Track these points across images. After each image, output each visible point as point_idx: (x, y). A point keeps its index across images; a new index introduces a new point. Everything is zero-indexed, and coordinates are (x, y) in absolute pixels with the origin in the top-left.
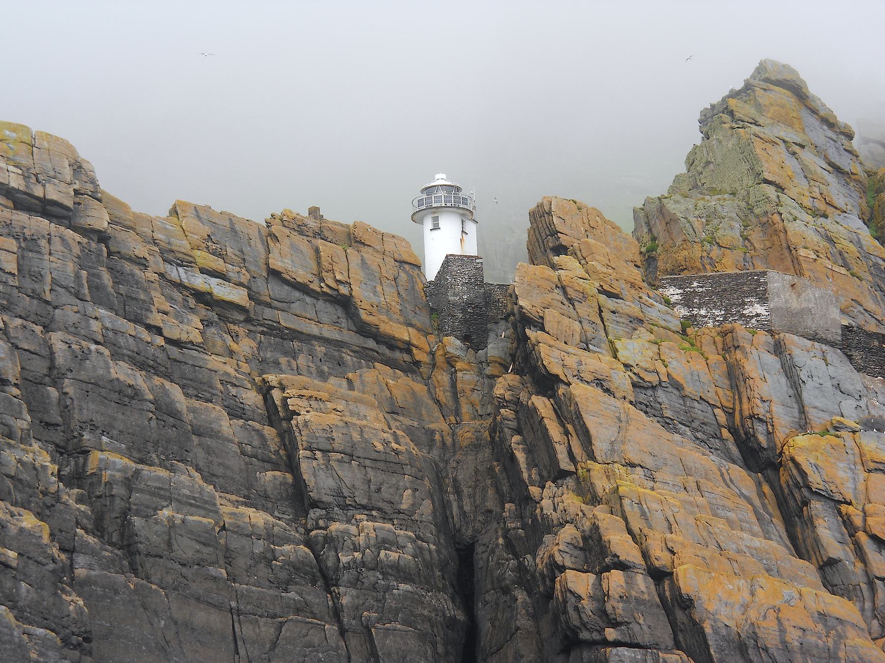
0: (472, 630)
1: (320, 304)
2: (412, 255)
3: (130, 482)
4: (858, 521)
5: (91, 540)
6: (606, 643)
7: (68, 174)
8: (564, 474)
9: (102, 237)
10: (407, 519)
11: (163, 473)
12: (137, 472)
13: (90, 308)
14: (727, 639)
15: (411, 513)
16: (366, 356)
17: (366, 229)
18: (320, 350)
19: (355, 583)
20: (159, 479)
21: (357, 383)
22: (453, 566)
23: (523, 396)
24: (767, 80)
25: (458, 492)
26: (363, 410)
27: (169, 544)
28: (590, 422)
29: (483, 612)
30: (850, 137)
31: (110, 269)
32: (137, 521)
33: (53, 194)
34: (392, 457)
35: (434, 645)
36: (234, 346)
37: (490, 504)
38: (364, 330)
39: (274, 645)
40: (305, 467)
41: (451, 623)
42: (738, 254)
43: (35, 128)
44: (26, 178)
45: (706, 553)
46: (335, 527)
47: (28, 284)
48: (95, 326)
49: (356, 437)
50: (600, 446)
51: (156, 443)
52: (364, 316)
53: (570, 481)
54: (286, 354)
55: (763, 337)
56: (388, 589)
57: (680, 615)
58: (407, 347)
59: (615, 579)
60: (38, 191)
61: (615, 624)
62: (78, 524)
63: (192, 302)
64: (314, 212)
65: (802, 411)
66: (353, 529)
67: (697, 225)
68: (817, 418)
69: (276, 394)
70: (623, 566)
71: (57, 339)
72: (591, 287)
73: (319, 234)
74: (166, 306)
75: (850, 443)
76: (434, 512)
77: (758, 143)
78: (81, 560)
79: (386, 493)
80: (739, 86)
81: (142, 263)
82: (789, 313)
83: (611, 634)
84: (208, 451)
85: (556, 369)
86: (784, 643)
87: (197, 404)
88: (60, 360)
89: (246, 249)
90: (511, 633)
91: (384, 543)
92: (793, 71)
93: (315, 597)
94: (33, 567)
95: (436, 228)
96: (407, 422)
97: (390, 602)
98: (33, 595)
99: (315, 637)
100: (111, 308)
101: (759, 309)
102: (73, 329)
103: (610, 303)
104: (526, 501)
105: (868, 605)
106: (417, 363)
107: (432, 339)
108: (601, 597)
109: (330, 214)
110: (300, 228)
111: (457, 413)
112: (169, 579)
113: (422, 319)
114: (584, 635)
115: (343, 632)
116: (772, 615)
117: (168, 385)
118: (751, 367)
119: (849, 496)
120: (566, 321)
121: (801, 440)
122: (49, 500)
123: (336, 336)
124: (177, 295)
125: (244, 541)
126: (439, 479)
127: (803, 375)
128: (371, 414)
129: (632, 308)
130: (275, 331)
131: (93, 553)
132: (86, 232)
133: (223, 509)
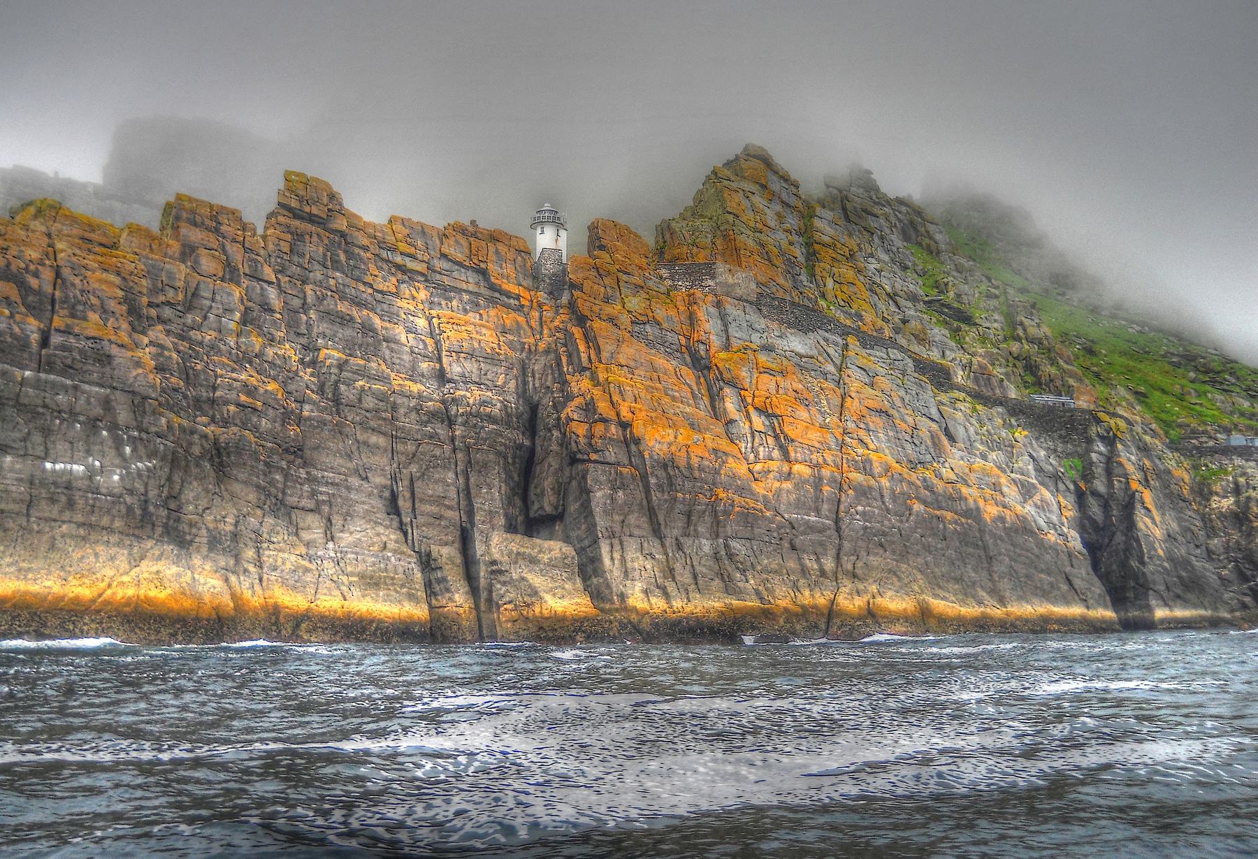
1: (469, 273)
2: (526, 247)
3: (341, 366)
4: (749, 400)
5: (314, 396)
6: (590, 461)
7: (325, 200)
9: (343, 235)
11: (362, 362)
12: (347, 361)
13: (330, 273)
14: (657, 461)
15: (502, 387)
16: (492, 302)
18: (466, 297)
21: (485, 317)
22: (526, 416)
23: (569, 326)
25: (533, 376)
26: (484, 331)
27: (360, 400)
28: (601, 342)
29: (538, 441)
31: (346, 252)
32: (343, 387)
33: (315, 211)
35: (505, 458)
37: (548, 384)
38: (493, 288)
39: (414, 455)
40: (445, 360)
42: (708, 252)
43: (309, 175)
45: (654, 415)
46: (458, 393)
47: (296, 259)
48: (332, 282)
49: (476, 345)
50: (605, 355)
52: (493, 279)
53: (588, 373)
54: (446, 299)
55: (710, 298)
56: (483, 427)
58: (518, 297)
59: (599, 429)
60: (307, 209)
61: (596, 451)
62: (307, 387)
63: (393, 270)
64: (473, 222)
65: (728, 339)
66: (468, 395)
67: (687, 235)
68: (736, 344)
69: (435, 321)
70: (605, 421)
72: (613, 269)
73: (474, 235)
74: (376, 273)
75: (751, 357)
76: (517, 387)
77: (726, 192)
80: (732, 158)
81: (366, 249)
82: (726, 285)
83: (594, 457)
84: (392, 351)
85: (587, 313)
86: (689, 464)
87: (388, 325)
88: (309, 300)
90: (548, 453)
91: (484, 403)
92: (763, 149)
93: (442, 431)
94: (271, 412)
95: (542, 233)
96: (511, 337)
97: (483, 435)
99: (438, 452)
101: (710, 283)
102: (320, 283)
103: (625, 277)
105: (750, 445)
106: (522, 306)
107: (532, 293)
109: (482, 224)
110: (463, 231)
111: (541, 333)
112: (358, 418)
113: (528, 282)
114: (579, 456)
115: (454, 450)
116: (684, 450)
117: (371, 315)
118: (701, 315)
119: (747, 386)
121: (723, 355)
122: (291, 375)
123: (476, 290)
124: (385, 266)
125: (405, 400)
126: (524, 369)
127: (730, 319)
129: (637, 280)
131: (314, 403)
132: (335, 231)
133: (394, 382)
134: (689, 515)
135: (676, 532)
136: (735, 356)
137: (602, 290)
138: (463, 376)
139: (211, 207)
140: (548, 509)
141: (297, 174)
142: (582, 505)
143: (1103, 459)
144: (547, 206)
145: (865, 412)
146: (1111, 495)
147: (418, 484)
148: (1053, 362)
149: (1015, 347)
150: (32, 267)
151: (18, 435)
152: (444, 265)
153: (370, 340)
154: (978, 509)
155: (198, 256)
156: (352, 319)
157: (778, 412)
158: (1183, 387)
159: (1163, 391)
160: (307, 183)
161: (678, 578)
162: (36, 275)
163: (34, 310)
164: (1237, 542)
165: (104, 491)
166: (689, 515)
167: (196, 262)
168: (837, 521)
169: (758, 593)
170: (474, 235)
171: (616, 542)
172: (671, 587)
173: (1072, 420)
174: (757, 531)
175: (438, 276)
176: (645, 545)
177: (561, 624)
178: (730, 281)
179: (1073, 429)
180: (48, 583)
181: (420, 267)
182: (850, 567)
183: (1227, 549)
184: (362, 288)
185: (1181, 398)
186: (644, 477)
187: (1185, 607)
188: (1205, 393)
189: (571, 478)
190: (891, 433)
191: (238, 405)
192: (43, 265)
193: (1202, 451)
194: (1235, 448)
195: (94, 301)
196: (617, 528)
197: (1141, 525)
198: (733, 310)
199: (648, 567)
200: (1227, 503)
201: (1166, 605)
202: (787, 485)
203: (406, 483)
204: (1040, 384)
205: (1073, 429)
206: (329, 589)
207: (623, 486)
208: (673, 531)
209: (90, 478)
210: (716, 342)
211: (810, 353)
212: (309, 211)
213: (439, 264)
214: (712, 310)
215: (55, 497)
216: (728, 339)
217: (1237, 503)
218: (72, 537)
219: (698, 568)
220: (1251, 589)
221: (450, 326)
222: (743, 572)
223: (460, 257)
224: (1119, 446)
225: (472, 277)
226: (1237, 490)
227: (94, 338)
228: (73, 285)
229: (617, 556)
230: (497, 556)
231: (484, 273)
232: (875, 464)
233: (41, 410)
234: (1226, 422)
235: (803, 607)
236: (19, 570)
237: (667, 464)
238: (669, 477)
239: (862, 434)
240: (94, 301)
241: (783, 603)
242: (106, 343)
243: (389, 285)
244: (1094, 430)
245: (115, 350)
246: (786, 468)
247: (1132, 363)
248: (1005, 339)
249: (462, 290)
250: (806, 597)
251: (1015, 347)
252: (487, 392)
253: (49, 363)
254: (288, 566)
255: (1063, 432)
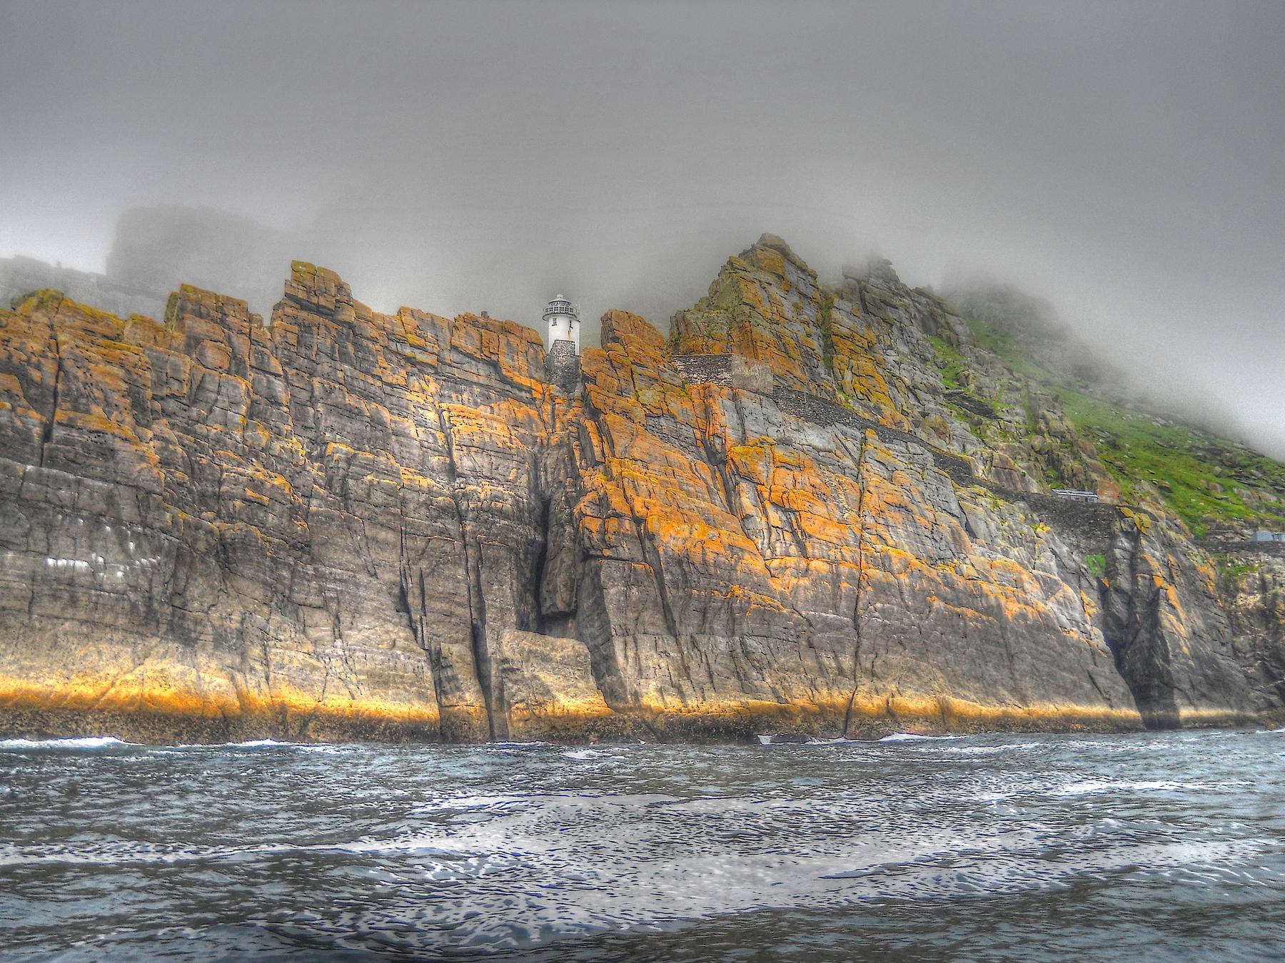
0: (544, 547)
1: (480, 365)
3: (350, 460)
4: (766, 495)
5: (322, 491)
6: (603, 557)
7: (333, 291)
8: (598, 463)
9: (351, 326)
10: (513, 484)
11: (371, 456)
13: (338, 365)
15: (514, 482)
16: (503, 394)
17: (512, 324)
18: (477, 390)
19: (476, 519)
20: (367, 459)
21: (496, 410)
23: (582, 419)
24: (765, 245)
25: (546, 471)
27: (369, 495)
28: (615, 435)
29: (550, 537)
30: (815, 278)
31: (354, 344)
32: (351, 482)
33: (322, 302)
34: (508, 451)
35: (517, 554)
36: (425, 387)
37: (561, 478)
38: (504, 380)
39: (424, 551)
40: (455, 454)
41: (532, 543)
42: (723, 343)
43: (317, 265)
44: (308, 292)
45: (668, 510)
46: (469, 487)
47: (303, 351)
48: (340, 374)
49: (487, 439)
51: (369, 439)
52: (504, 372)
53: (601, 467)
55: (726, 391)
56: (494, 523)
57: (648, 544)
58: (530, 390)
59: (613, 524)
60: (315, 300)
61: (610, 547)
62: (315, 482)
63: (403, 362)
64: (484, 314)
65: (744, 433)
66: (479, 489)
68: (752, 438)
69: (445, 414)
70: (618, 516)
71: (316, 382)
72: (627, 361)
78: (314, 502)
79: (501, 470)
80: (749, 248)
81: (374, 340)
83: (607, 553)
84: (401, 444)
85: (601, 406)
86: (704, 560)
87: (397, 418)
88: (316, 393)
89: (440, 334)
91: (495, 498)
92: (780, 239)
93: (452, 526)
94: (278, 506)
95: (555, 324)
97: (494, 530)
98: (276, 521)
99: (448, 548)
100: (352, 365)
101: (726, 375)
103: (639, 370)
104: (578, 477)
107: (545, 386)
108: (604, 532)
109: (493, 316)
111: (554, 427)
113: (540, 375)
114: (592, 552)
115: (465, 546)
117: (380, 408)
118: (717, 408)
120: (609, 379)
121: (739, 449)
122: (298, 469)
124: (394, 358)
125: (414, 494)
127: (746, 412)
128: (499, 426)
130: (449, 378)
131: (322, 498)
134: (704, 612)
135: (691, 630)
136: (752, 450)
137: (616, 382)
138: (474, 470)
139: (217, 297)
140: (561, 606)
141: (305, 265)
142: (595, 602)
143: (1127, 555)
144: (559, 297)
145: (884, 507)
146: (1135, 592)
147: (428, 580)
148: (1076, 456)
149: (1037, 441)
150: (34, 359)
151: (19, 530)
152: (455, 357)
153: (379, 434)
154: (999, 606)
155: (203, 348)
156: (360, 413)
157: (795, 507)
158: (1208, 481)
159: (1189, 486)
160: (314, 273)
161: (693, 676)
162: (38, 367)
163: (35, 403)
164: (1264, 640)
165: (107, 587)
166: (704, 612)
167: (202, 354)
168: (856, 618)
169: (774, 691)
170: (485, 327)
171: (630, 639)
172: (686, 686)
173: (1095, 516)
174: (774, 628)
175: (448, 369)
176: (660, 642)
177: (574, 723)
178: (747, 373)
179: (1097, 524)
180: (50, 682)
181: (430, 359)
182: (868, 665)
183: (1254, 647)
184: (371, 380)
185: (1206, 493)
186: (659, 574)
187: (1210, 707)
188: (1231, 488)
189: (584, 574)
190: (910, 529)
191: (245, 500)
192: (46, 357)
193: (1227, 547)
194: (1262, 544)
195: (97, 393)
196: (631, 626)
197: (1165, 623)
198: (748, 403)
199: (663, 665)
200: (1254, 600)
201: (1191, 704)
202: (805, 582)
203: (416, 579)
204: (1063, 478)
205: (1097, 524)
206: (337, 688)
207: (637, 583)
208: (688, 628)
209: (93, 574)
210: (732, 435)
211: (828, 447)
212: (316, 302)
213: (449, 356)
214: (728, 403)
215: (58, 594)
216: (744, 433)
217: (1264, 600)
218: (74, 634)
219: (714, 667)
220: (1277, 687)
221: (460, 419)
222: (760, 670)
223: (471, 349)
224: (1144, 542)
225: (483, 370)
226: (1264, 587)
227: (97, 432)
228: (76, 377)
229: (631, 654)
230: (508, 654)
231: (495, 365)
232: (894, 560)
233: (43, 505)
234: (1252, 517)
235: (821, 706)
236: (21, 669)
237: (682, 561)
238: (684, 574)
239: (881, 529)
240: (97, 393)
241: (800, 702)
242: (109, 436)
243: (398, 377)
244: (1117, 526)
245: (118, 444)
246: (803, 564)
247: (1156, 458)
248: (1027, 433)
249: (473, 383)
250: (824, 696)
251: (1037, 441)
252: (499, 487)
253: (51, 458)
254: (295, 664)
255: (1086, 528)
